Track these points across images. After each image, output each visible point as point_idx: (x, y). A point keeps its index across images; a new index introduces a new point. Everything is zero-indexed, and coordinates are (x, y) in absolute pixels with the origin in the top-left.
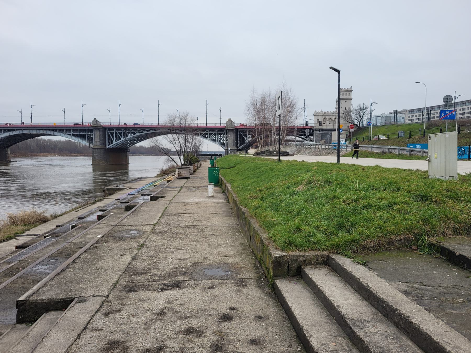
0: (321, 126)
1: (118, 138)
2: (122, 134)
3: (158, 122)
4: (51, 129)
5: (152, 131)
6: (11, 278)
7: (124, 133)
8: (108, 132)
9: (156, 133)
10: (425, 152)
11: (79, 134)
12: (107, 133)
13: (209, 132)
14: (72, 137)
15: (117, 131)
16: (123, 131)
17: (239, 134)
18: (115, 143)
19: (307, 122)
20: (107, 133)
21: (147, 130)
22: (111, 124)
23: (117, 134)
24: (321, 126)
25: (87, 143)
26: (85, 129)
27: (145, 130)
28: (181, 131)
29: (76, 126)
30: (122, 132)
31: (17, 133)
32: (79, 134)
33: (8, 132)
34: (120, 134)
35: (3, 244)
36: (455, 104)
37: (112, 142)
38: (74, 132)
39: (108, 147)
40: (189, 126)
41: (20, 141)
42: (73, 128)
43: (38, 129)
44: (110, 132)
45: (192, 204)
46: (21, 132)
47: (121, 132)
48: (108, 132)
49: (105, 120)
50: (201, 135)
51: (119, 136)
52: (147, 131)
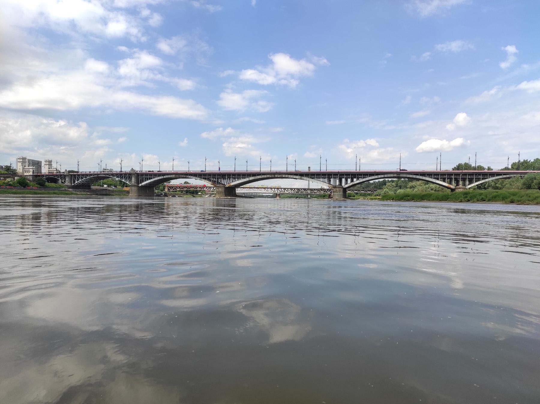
0: (309, 167)
1: (82, 178)
3: (270, 170)
6: (125, 286)
8: (77, 177)
10: (217, 215)
13: (217, 176)
18: (76, 182)
24: (309, 167)
28: (110, 175)
29: (201, 172)
33: (495, 176)
37: (75, 182)
38: (242, 176)
39: (140, 185)
45: (431, 250)
46: (165, 177)
49: (137, 169)
52: (93, 176)
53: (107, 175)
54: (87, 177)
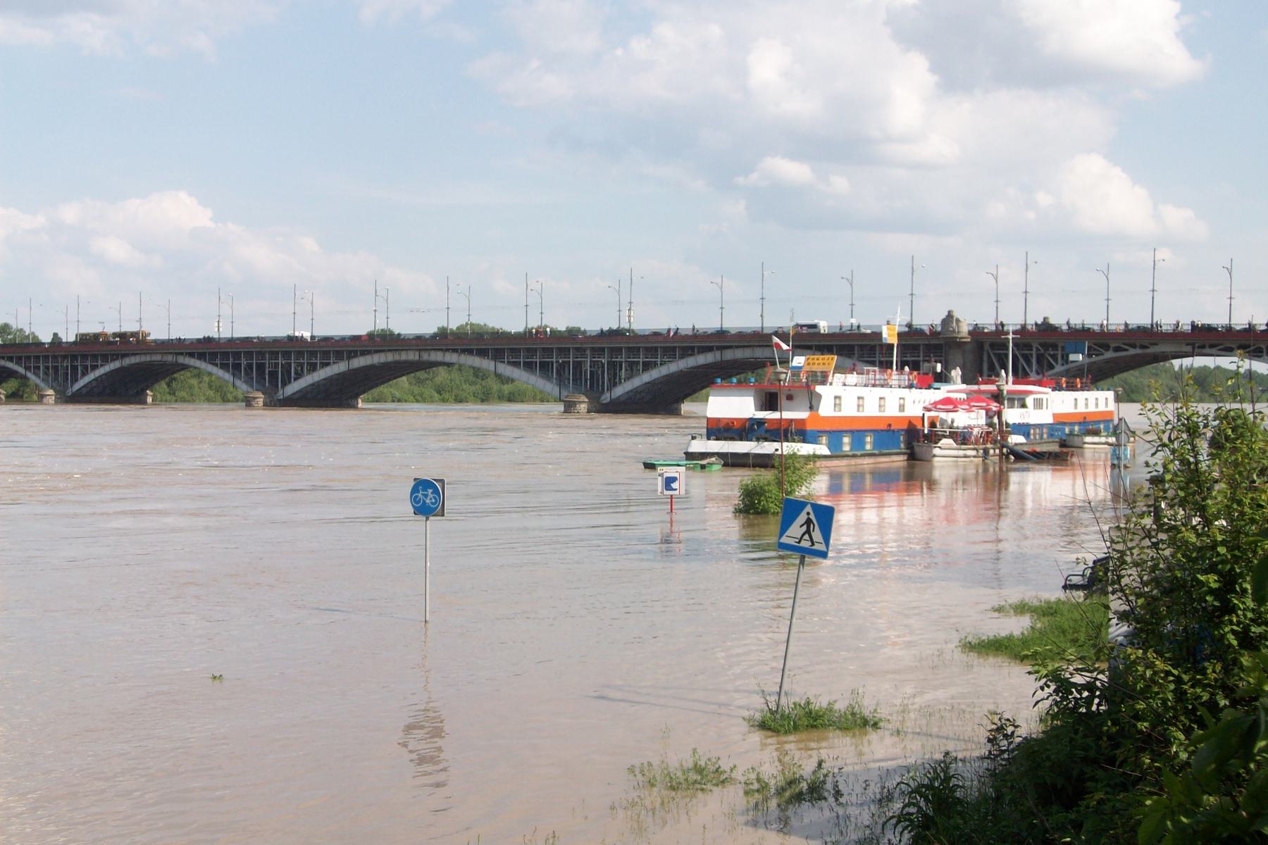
2: (1034, 361)
4: (816, 346)
5: (1132, 352)
7: (1040, 359)
8: (989, 357)
9: (1147, 355)
11: (641, 360)
12: (985, 358)
14: (220, 370)
15: (1018, 350)
16: (1038, 349)
17: (267, 372)
19: (880, 728)
20: (985, 358)
21: (1113, 345)
22: (762, 331)
23: (1018, 359)
25: (555, 387)
26: (621, 348)
27: (1107, 347)
30: (1034, 352)
31: (718, 358)
32: (641, 360)
34: (1027, 359)
35: (881, 844)
36: (904, 454)
40: (1083, 327)
41: (392, 377)
42: (662, 345)
43: (434, 349)
44: (995, 354)
47: (1031, 355)
48: (989, 357)
50: (1057, 363)
51: (1022, 365)
52: (1117, 349)
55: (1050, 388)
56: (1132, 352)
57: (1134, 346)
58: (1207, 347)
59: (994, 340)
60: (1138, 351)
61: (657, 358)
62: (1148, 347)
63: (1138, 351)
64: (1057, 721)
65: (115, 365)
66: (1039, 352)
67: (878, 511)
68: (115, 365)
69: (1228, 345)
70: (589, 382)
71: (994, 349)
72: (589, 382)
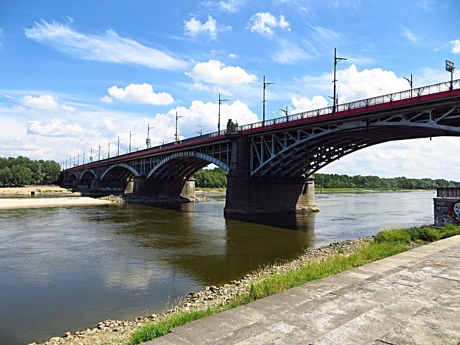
21: (314, 129)
53: (382, 120)
54: (294, 142)
55: (351, 178)
56: (326, 132)
57: (327, 128)
58: (379, 120)
59: (294, 265)
60: (330, 131)
61: (272, 140)
62: (336, 127)
63: (330, 131)
64: (203, 21)
65: (167, 159)
66: (290, 139)
67: (187, 210)
68: (167, 159)
69: (396, 116)
70: (451, 97)
71: (267, 140)
72: (451, 97)
